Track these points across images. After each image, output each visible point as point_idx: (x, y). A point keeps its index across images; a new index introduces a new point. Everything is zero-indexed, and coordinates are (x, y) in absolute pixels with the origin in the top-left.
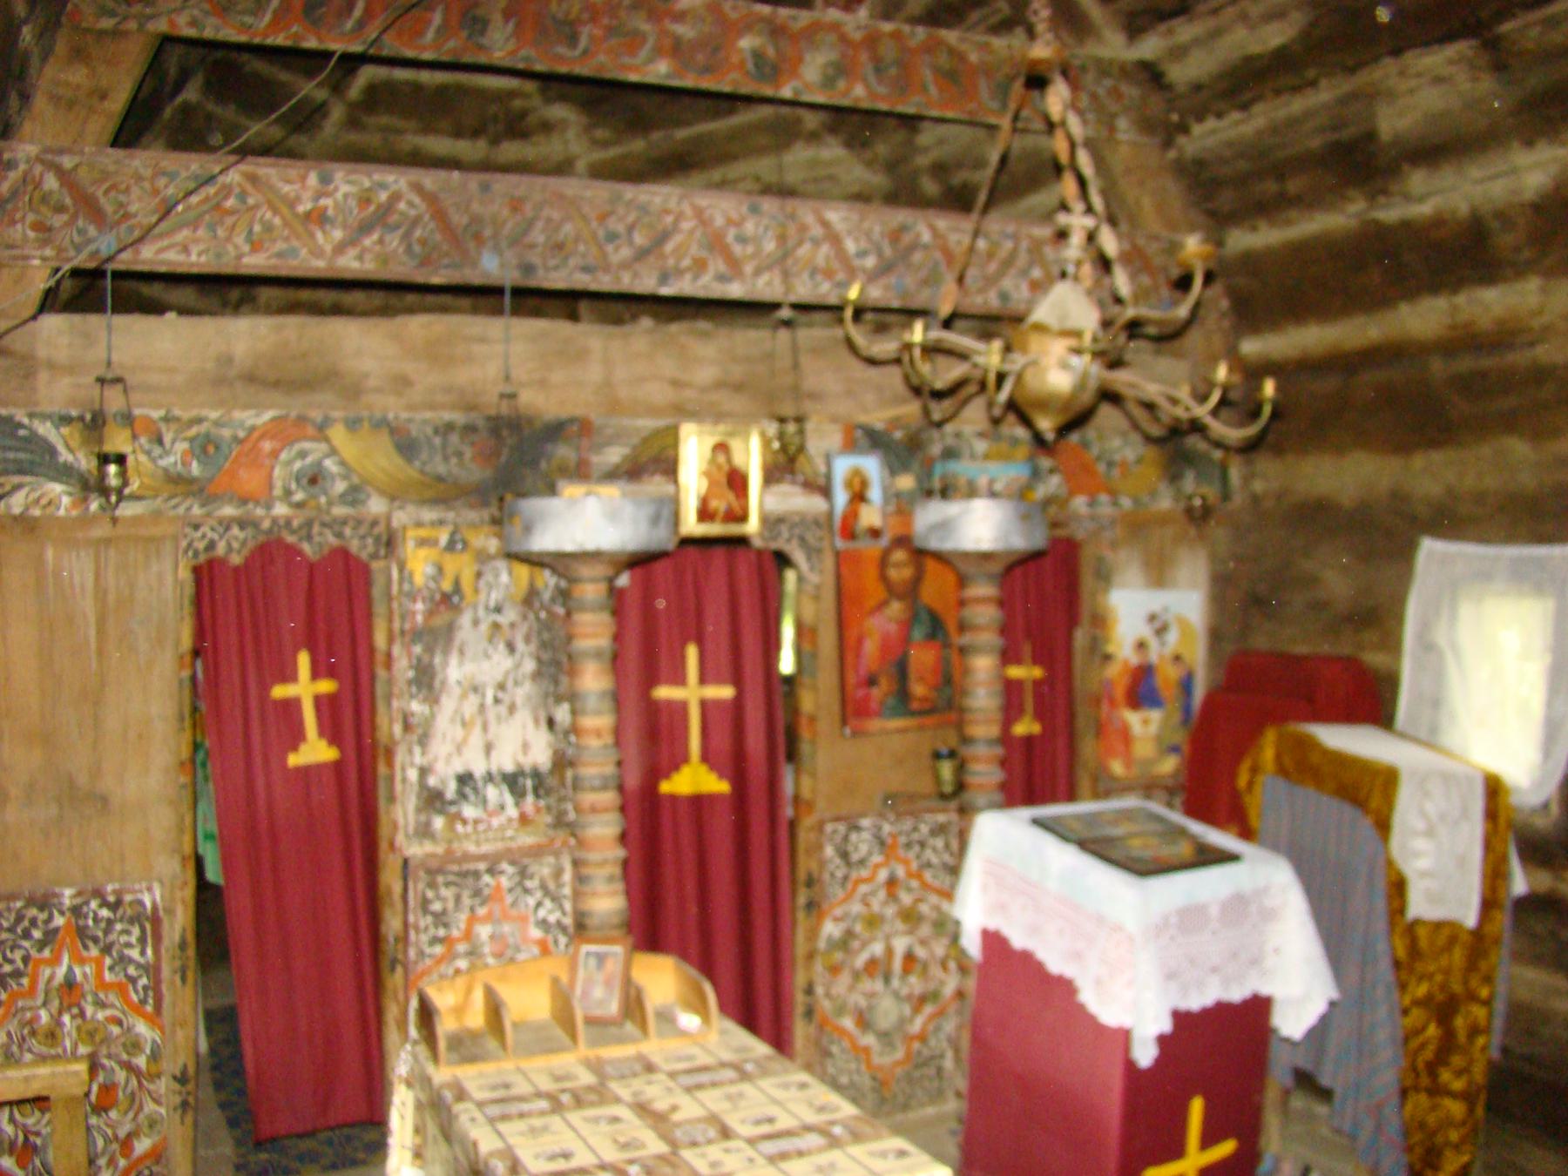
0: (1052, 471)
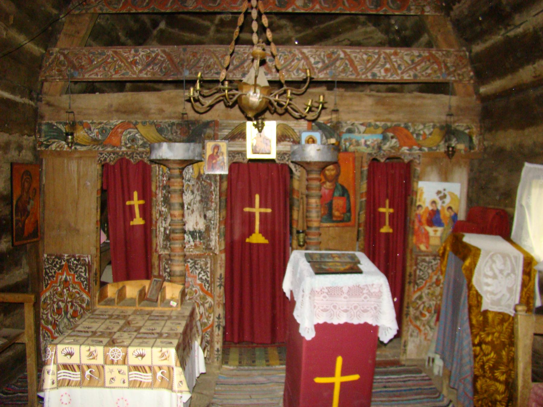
0: (392, 138)
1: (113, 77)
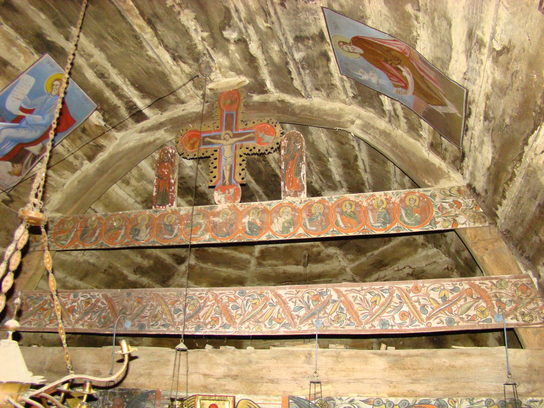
1: (47, 327)
